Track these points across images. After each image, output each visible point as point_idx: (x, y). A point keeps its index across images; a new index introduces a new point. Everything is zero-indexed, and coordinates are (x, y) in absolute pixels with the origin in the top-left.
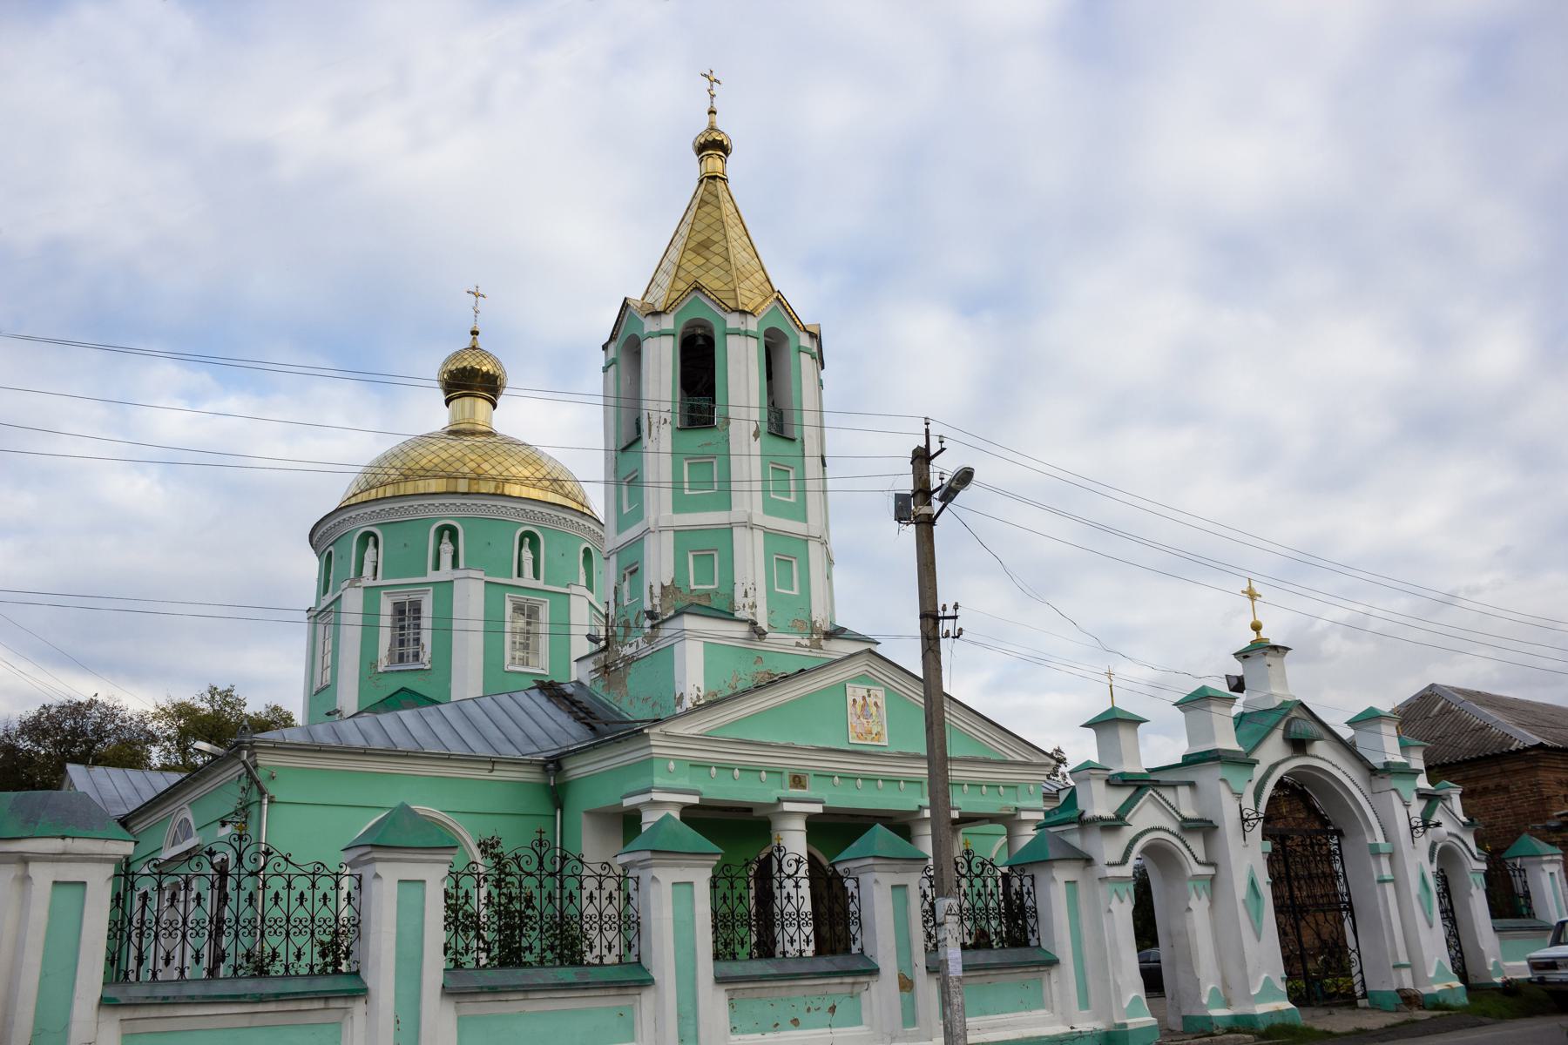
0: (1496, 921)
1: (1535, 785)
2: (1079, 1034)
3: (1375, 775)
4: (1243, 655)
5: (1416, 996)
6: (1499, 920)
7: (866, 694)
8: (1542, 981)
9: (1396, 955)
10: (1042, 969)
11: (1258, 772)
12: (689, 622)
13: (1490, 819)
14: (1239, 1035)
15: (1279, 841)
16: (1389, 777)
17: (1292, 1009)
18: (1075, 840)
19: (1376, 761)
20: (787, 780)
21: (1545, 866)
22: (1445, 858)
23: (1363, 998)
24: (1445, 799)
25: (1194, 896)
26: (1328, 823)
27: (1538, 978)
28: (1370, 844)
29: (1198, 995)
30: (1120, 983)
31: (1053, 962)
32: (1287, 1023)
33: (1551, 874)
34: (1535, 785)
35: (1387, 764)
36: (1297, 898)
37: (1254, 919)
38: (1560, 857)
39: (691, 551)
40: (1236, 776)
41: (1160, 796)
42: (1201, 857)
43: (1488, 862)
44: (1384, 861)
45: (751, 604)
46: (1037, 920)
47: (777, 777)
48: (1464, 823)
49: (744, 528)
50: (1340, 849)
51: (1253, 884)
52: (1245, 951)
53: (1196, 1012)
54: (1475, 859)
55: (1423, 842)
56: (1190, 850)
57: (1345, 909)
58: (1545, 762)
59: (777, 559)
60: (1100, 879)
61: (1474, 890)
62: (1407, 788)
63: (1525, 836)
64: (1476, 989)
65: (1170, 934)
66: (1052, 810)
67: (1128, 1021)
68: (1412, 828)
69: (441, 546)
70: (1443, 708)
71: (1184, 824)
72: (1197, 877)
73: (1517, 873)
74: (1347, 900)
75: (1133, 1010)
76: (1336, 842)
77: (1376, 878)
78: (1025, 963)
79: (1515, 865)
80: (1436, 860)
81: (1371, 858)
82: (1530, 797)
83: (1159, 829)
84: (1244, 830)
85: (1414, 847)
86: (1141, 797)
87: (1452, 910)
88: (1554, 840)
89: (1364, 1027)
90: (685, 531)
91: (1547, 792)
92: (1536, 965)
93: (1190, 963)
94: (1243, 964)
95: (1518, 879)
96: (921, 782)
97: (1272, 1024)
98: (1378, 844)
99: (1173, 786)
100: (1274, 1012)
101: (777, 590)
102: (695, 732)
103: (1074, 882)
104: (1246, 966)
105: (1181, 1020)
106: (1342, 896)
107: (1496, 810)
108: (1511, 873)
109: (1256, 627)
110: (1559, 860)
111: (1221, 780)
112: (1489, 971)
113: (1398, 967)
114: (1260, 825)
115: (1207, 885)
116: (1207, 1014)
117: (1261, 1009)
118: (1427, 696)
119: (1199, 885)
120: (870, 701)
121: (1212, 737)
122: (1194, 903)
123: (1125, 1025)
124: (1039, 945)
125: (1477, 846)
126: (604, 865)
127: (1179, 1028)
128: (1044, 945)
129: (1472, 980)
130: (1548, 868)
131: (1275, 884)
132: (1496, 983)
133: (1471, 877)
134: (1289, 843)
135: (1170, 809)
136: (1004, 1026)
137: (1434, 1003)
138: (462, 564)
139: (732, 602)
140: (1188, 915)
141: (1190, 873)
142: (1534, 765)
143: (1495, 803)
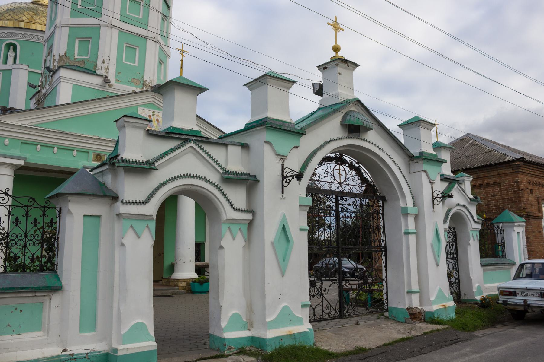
0: (483, 259)
1: (515, 182)
2: (71, 357)
3: (413, 160)
4: (323, 68)
5: (420, 313)
6: (485, 259)
7: (151, 114)
8: (505, 303)
9: (409, 284)
10: (37, 294)
12: (63, 73)
13: (488, 201)
16: (421, 162)
19: (415, 152)
20: (92, 156)
21: (515, 229)
24: (461, 184)
30: (122, 311)
31: (57, 288)
32: (297, 344)
33: (518, 233)
34: (515, 182)
35: (421, 153)
38: (524, 224)
39: (77, 38)
43: (483, 224)
44: (411, 220)
45: (106, 67)
47: (85, 155)
48: (470, 199)
49: (107, 27)
51: (437, 232)
55: (441, 209)
58: (522, 169)
59: (126, 46)
61: (471, 242)
62: (433, 170)
63: (507, 211)
67: (120, 347)
68: (434, 198)
69: (9, 54)
73: (499, 232)
77: (403, 231)
78: (10, 289)
79: (498, 227)
82: (513, 189)
85: (433, 211)
87: (457, 253)
88: (522, 214)
90: (76, 27)
91: (522, 186)
92: (504, 292)
93: (217, 293)
95: (499, 235)
96: (88, 152)
97: (280, 347)
98: (407, 207)
101: (124, 61)
102: (26, 124)
103: (99, 216)
107: (492, 196)
108: (496, 231)
109: (336, 49)
110: (523, 225)
111: (266, 142)
112: (473, 292)
113: (410, 292)
115: (245, 228)
116: (223, 337)
118: (465, 138)
119: (235, 228)
121: (266, 109)
123: (116, 350)
125: (477, 214)
126: (31, 200)
129: (463, 297)
130: (517, 230)
132: (476, 300)
133: (471, 233)
135: (212, 162)
137: (431, 319)
138: (18, 62)
139: (96, 66)
140: (220, 251)
142: (517, 170)
143: (493, 192)
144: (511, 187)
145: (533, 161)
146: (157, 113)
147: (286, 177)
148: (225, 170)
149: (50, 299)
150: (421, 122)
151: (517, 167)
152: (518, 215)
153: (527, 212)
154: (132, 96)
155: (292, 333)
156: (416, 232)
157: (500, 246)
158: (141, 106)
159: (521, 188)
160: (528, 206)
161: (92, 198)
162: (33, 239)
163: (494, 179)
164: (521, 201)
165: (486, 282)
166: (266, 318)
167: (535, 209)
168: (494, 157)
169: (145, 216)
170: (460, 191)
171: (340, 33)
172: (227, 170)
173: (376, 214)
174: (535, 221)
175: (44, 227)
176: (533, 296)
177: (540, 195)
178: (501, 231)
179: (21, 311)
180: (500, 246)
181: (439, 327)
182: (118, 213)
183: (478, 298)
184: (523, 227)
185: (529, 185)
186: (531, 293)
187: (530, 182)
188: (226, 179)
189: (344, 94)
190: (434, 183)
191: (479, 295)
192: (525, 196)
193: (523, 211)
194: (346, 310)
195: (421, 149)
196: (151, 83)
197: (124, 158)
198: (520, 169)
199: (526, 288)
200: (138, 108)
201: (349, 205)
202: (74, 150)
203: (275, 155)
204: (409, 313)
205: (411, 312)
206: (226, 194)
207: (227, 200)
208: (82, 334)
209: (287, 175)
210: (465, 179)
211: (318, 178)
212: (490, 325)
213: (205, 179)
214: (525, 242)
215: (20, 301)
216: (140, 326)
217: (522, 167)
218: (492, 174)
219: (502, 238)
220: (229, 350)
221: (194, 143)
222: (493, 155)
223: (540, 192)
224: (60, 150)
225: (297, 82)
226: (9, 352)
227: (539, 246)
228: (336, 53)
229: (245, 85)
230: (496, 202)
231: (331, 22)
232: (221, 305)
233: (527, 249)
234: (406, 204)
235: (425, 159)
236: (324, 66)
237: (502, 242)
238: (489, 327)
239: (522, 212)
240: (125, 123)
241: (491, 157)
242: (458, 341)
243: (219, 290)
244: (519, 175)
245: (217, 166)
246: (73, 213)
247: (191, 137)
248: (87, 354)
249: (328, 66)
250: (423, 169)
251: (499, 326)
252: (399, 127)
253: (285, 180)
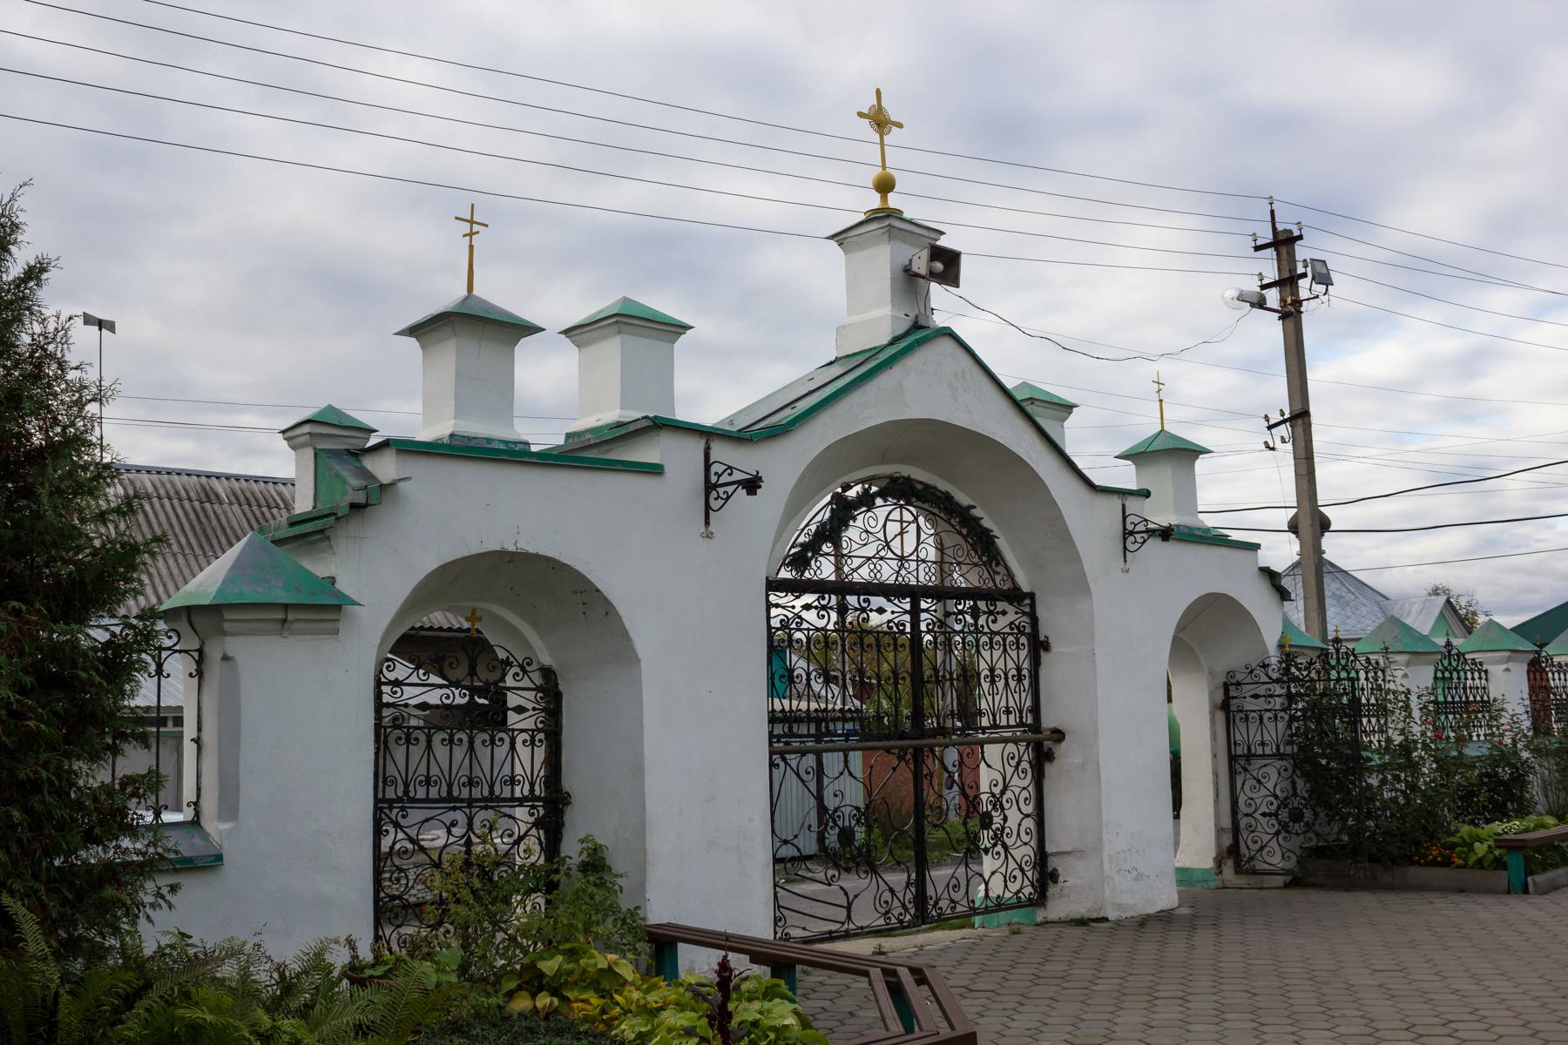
109: (885, 186)
147: (716, 486)
171: (893, 136)
194: (932, 902)
211: (848, 550)
225: (1287, 886)
253: (714, 494)
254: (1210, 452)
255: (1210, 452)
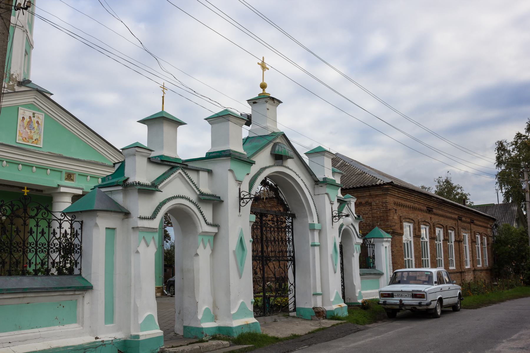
0: (361, 269)
1: (384, 203)
2: (102, 343)
3: (318, 184)
4: (253, 102)
5: (323, 311)
7: (32, 116)
8: (385, 303)
9: (315, 288)
10: (77, 293)
11: (254, 170)
14: (220, 342)
15: (259, 217)
16: (325, 186)
17: (256, 322)
18: (119, 198)
19: (320, 177)
21: (384, 243)
22: (345, 234)
23: (294, 311)
25: (201, 246)
26: (288, 209)
27: (383, 302)
28: (309, 223)
29: (196, 313)
31: (88, 288)
32: (252, 332)
33: (386, 247)
34: (384, 203)
35: (325, 179)
36: (265, 252)
37: (239, 265)
38: (390, 239)
40: (240, 170)
41: (187, 175)
42: (210, 220)
44: (316, 234)
46: (81, 255)
48: (355, 218)
50: (292, 225)
51: (241, 241)
52: (231, 284)
53: (193, 324)
54: (358, 237)
55: (337, 225)
56: (202, 215)
57: (290, 260)
58: (390, 192)
60: (133, 228)
63: (377, 228)
64: (352, 306)
65: (182, 271)
66: (106, 177)
67: (140, 334)
68: (333, 217)
70: (342, 163)
71: (201, 197)
72: (205, 233)
74: (292, 255)
75: (145, 326)
76: (291, 221)
77: (310, 244)
78: (61, 288)
79: (370, 242)
80: (341, 236)
81: (309, 232)
82: (382, 209)
83: (182, 197)
84: (240, 205)
85: (332, 228)
86: (173, 174)
88: (389, 231)
89: (297, 334)
91: (389, 207)
92: (383, 295)
93: (193, 292)
94: (228, 293)
96: (61, 172)
98: (314, 224)
99: (197, 170)
100: (245, 325)
103: (114, 229)
104: (230, 294)
105: (183, 328)
106: (290, 252)
107: (364, 214)
109: (263, 86)
113: (315, 295)
114: (250, 203)
115: (212, 239)
116: (200, 327)
117: (236, 323)
119: (206, 239)
120: (34, 120)
121: (227, 142)
122: (201, 251)
123: (137, 336)
124: (80, 274)
127: (181, 333)
128: (83, 275)
131: (254, 243)
133: (355, 246)
134: (264, 218)
135: (192, 185)
136: (36, 339)
137: (333, 316)
140: (196, 258)
141: (200, 230)
142: (386, 193)
144: (380, 207)
145: (399, 185)
146: (38, 115)
148: (201, 192)
149: (83, 297)
150: (325, 152)
151: (387, 189)
152: (386, 232)
153: (392, 230)
154: (13, 95)
155: (249, 323)
156: (319, 245)
157: (371, 258)
158: (21, 106)
159: (389, 208)
160: (394, 224)
161: (113, 213)
162: (31, 249)
163: (366, 199)
164: (388, 220)
165: (363, 289)
166: (231, 311)
167: (398, 227)
168: (366, 179)
169: (153, 229)
170: (348, 210)
172: (202, 192)
173: (287, 228)
174: (398, 238)
175: (61, 238)
176: (406, 297)
177: (402, 215)
178: (372, 246)
179: (63, 307)
180: (371, 258)
181: (339, 322)
182: (136, 226)
183: (360, 301)
184: (389, 242)
185: (394, 206)
186: (405, 295)
187: (395, 203)
188: (203, 199)
189: (271, 128)
190: (333, 204)
191: (360, 299)
192: (391, 214)
193: (390, 228)
195: (324, 175)
196: (17, 78)
197: (140, 182)
198: (388, 191)
199: (402, 290)
200: (18, 108)
201: (269, 221)
202: (20, 164)
203: (235, 181)
204: (315, 312)
205: (317, 311)
206: (202, 212)
207: (202, 217)
208: (106, 326)
209: (244, 197)
210: (352, 200)
212: (373, 321)
213: (189, 199)
214: (391, 255)
215: (64, 298)
216: (150, 317)
217: (391, 190)
218: (365, 195)
219: (373, 251)
220: (205, 337)
221: (181, 170)
222: (365, 178)
223: (402, 212)
224: (25, 167)
226: (60, 339)
227: (400, 259)
228: (263, 90)
229: (206, 119)
230: (366, 220)
231: (260, 62)
232: (197, 301)
233: (392, 261)
234: (313, 221)
235: (328, 184)
236: (254, 101)
237: (373, 255)
238: (373, 323)
239: (389, 229)
240: (136, 153)
241: (364, 179)
242: (359, 330)
243: (195, 289)
244: (388, 197)
245: (195, 189)
246: (99, 226)
247: (177, 164)
248: (112, 340)
249: (258, 102)
250: (327, 192)
251: (380, 322)
252: (305, 155)
254: (186, 124)
255: (186, 124)
